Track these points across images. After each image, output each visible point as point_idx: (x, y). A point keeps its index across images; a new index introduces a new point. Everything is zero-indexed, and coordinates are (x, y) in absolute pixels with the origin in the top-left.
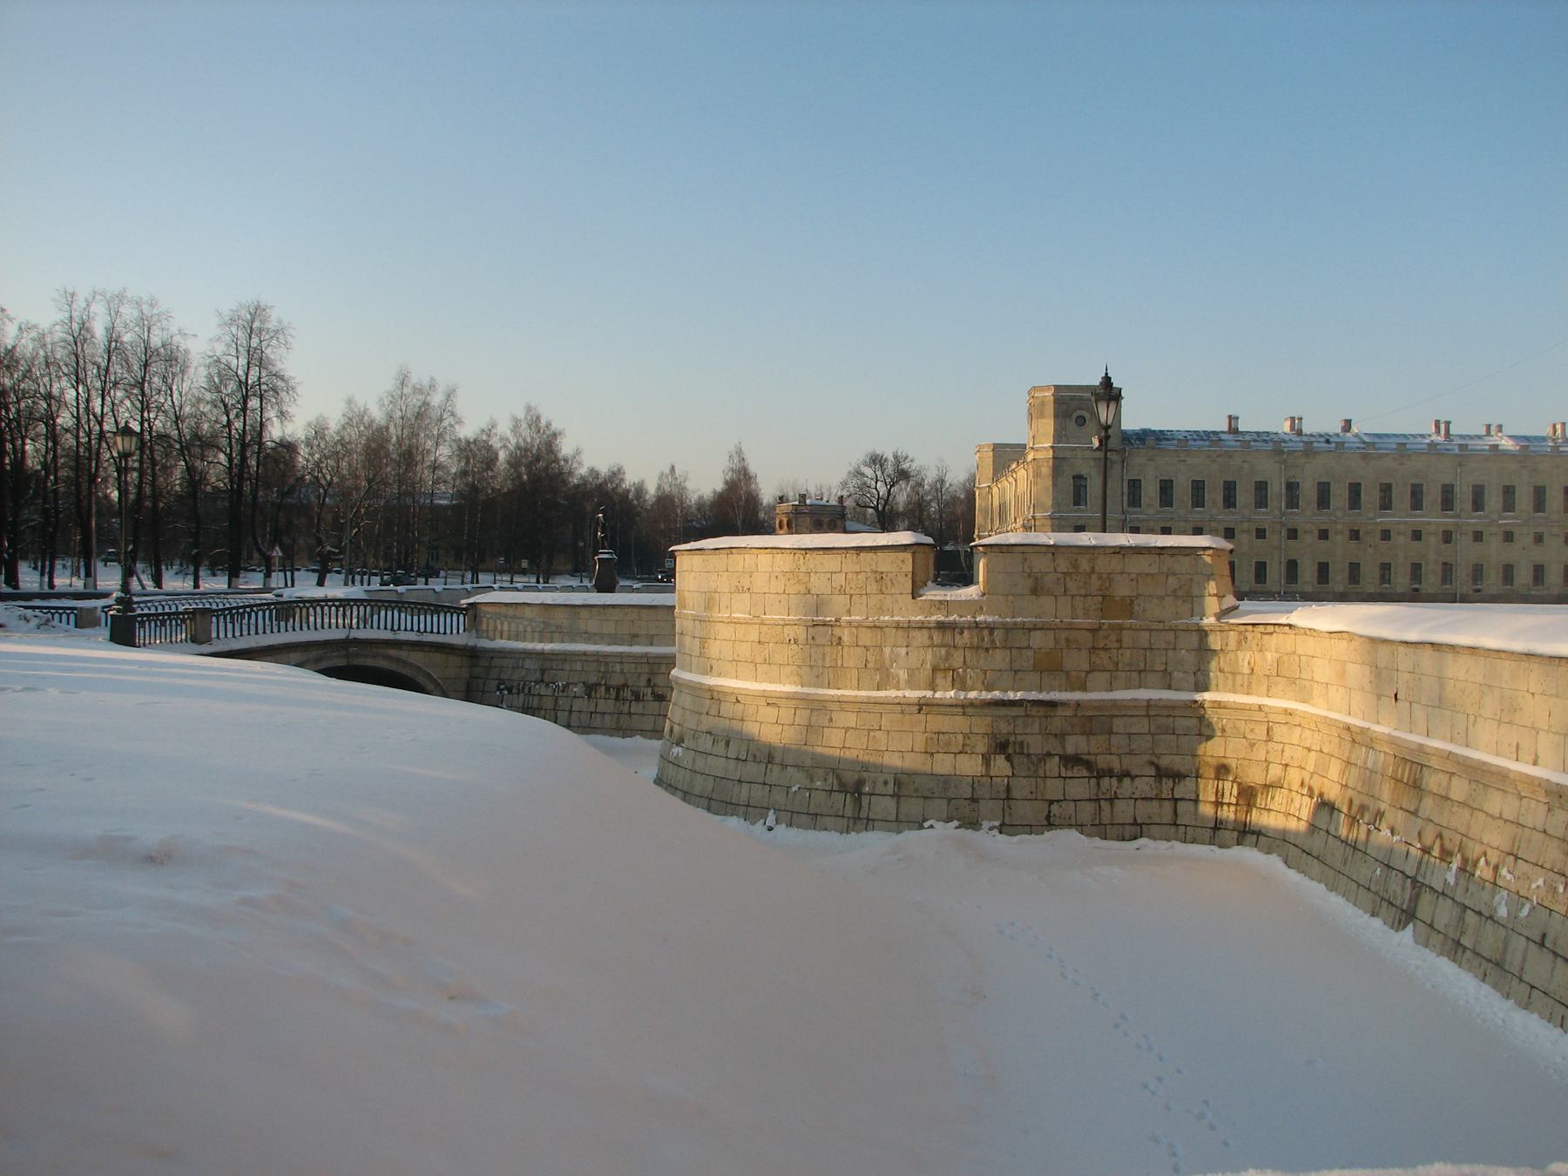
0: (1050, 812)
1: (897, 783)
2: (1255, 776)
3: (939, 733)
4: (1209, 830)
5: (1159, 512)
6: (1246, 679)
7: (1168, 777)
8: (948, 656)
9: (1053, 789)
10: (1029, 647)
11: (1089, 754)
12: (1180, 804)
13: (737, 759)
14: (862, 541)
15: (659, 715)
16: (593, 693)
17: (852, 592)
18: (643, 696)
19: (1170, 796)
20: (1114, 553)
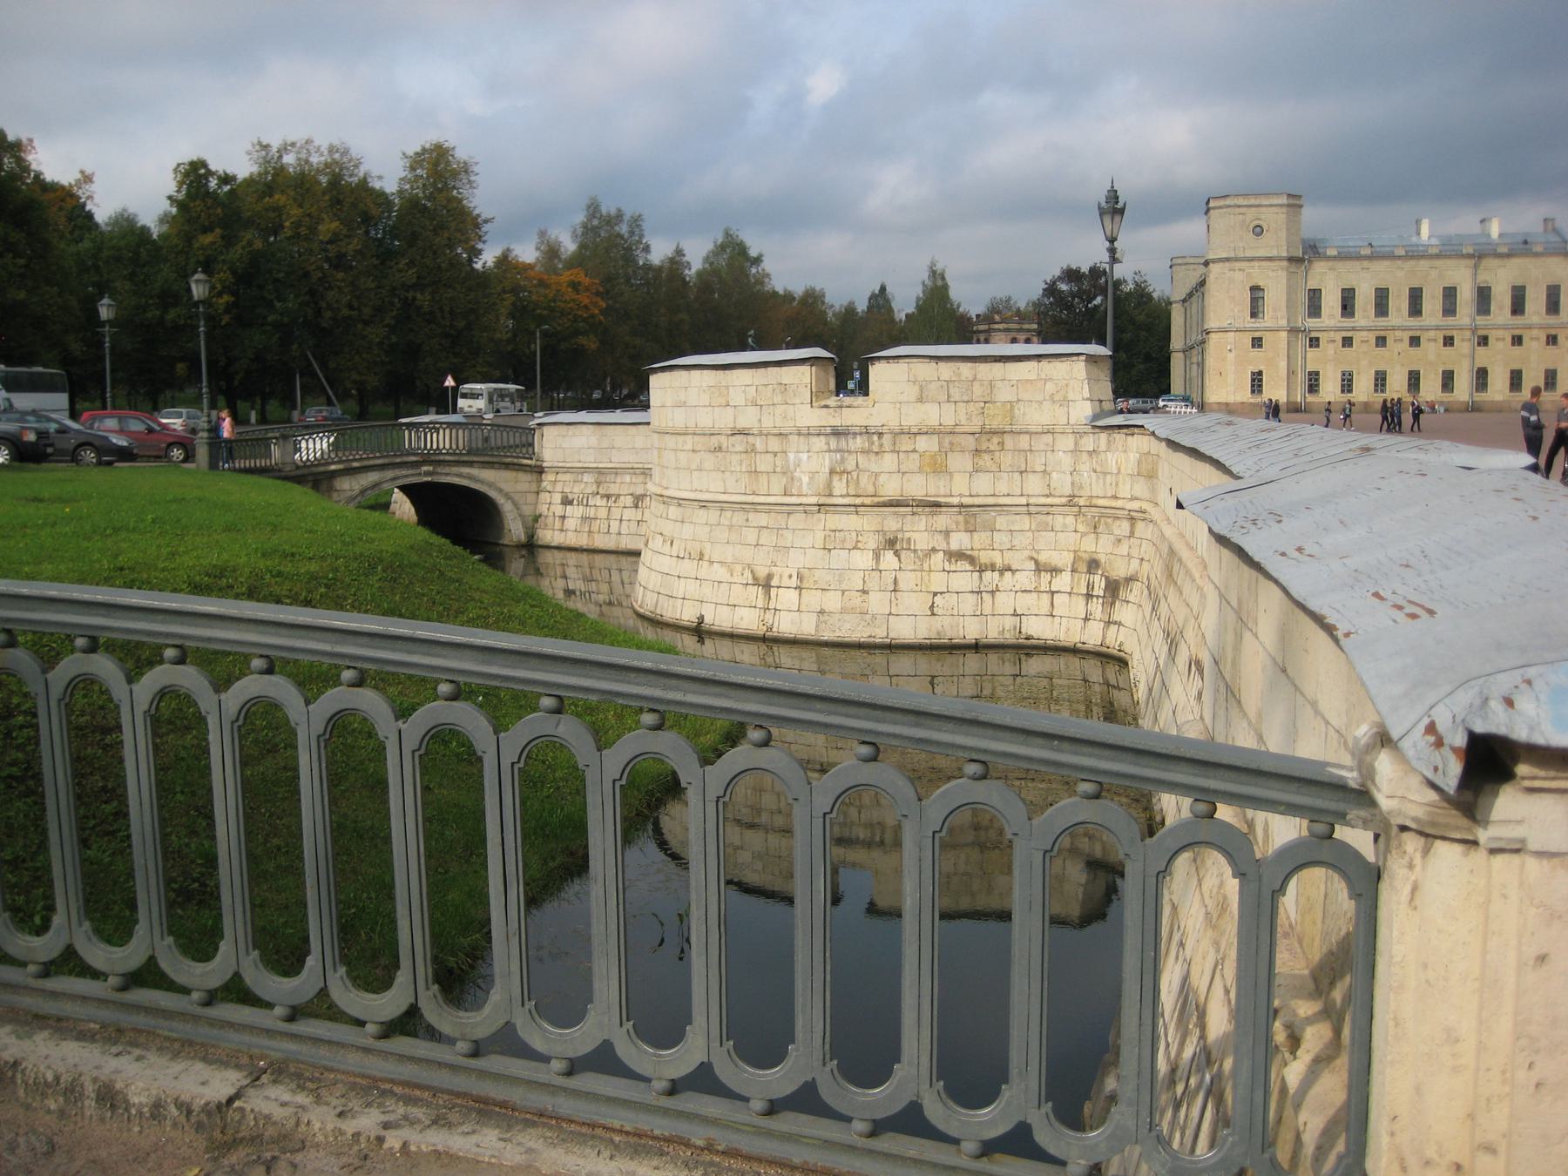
0: (933, 603)
1: (800, 577)
2: (1120, 571)
5: (1339, 322)
7: (1046, 571)
9: (938, 582)
10: (914, 451)
11: (972, 549)
12: (1055, 595)
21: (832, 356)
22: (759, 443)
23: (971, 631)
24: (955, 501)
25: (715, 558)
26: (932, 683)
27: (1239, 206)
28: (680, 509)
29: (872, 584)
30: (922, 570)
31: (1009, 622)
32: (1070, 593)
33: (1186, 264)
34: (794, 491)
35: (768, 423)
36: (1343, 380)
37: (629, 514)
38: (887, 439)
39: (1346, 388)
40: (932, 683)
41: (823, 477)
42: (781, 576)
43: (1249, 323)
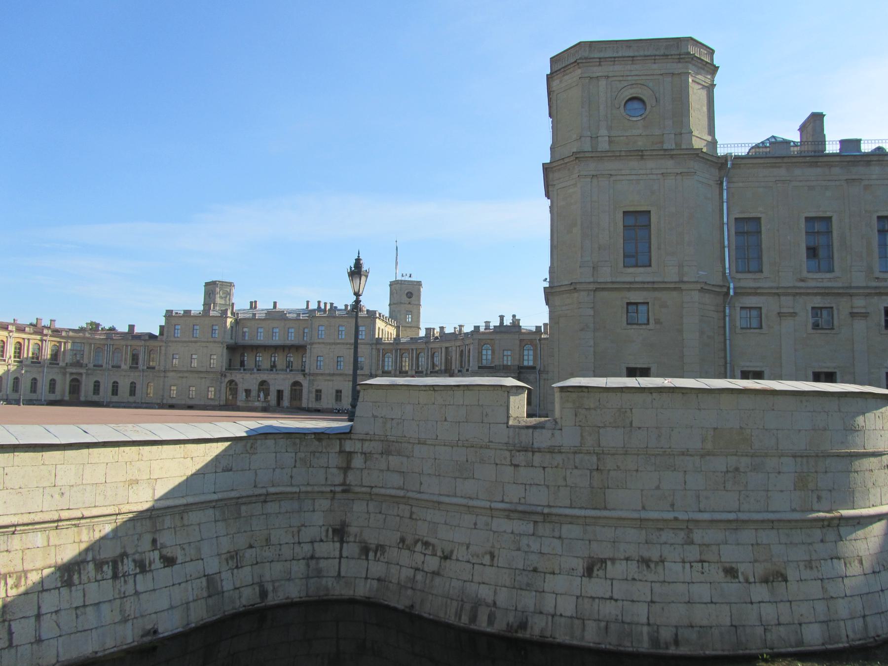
15: (173, 585)
16: (76, 577)
18: (150, 565)
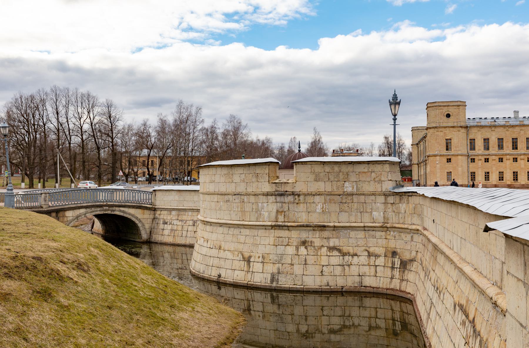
1: (263, 257)
2: (407, 256)
3: (279, 237)
4: (389, 279)
5: (483, 152)
6: (403, 215)
8: (282, 207)
9: (324, 260)
12: (378, 267)
13: (210, 248)
14: (505, 177)
16: (196, 224)
17: (248, 181)
19: (374, 264)
20: (349, 164)
21: (276, 161)
22: (246, 198)
23: (340, 282)
24: (332, 224)
25: (226, 249)
26: (322, 310)
27: (440, 106)
28: (212, 227)
29: (296, 261)
30: (317, 255)
31: (357, 279)
32: (384, 266)
33: (418, 129)
34: (261, 220)
35: (250, 190)
36: (485, 176)
37: (190, 228)
38: (302, 198)
39: (487, 179)
40: (322, 310)
41: (274, 214)
42: (255, 257)
43: (444, 152)
